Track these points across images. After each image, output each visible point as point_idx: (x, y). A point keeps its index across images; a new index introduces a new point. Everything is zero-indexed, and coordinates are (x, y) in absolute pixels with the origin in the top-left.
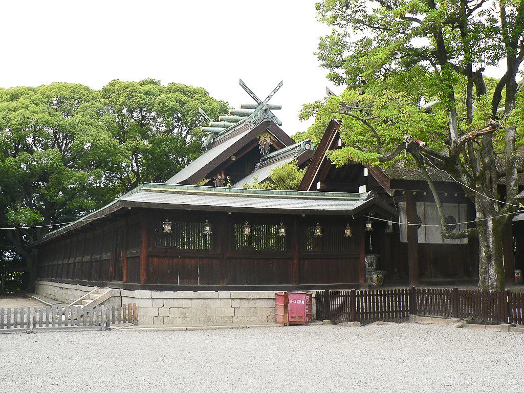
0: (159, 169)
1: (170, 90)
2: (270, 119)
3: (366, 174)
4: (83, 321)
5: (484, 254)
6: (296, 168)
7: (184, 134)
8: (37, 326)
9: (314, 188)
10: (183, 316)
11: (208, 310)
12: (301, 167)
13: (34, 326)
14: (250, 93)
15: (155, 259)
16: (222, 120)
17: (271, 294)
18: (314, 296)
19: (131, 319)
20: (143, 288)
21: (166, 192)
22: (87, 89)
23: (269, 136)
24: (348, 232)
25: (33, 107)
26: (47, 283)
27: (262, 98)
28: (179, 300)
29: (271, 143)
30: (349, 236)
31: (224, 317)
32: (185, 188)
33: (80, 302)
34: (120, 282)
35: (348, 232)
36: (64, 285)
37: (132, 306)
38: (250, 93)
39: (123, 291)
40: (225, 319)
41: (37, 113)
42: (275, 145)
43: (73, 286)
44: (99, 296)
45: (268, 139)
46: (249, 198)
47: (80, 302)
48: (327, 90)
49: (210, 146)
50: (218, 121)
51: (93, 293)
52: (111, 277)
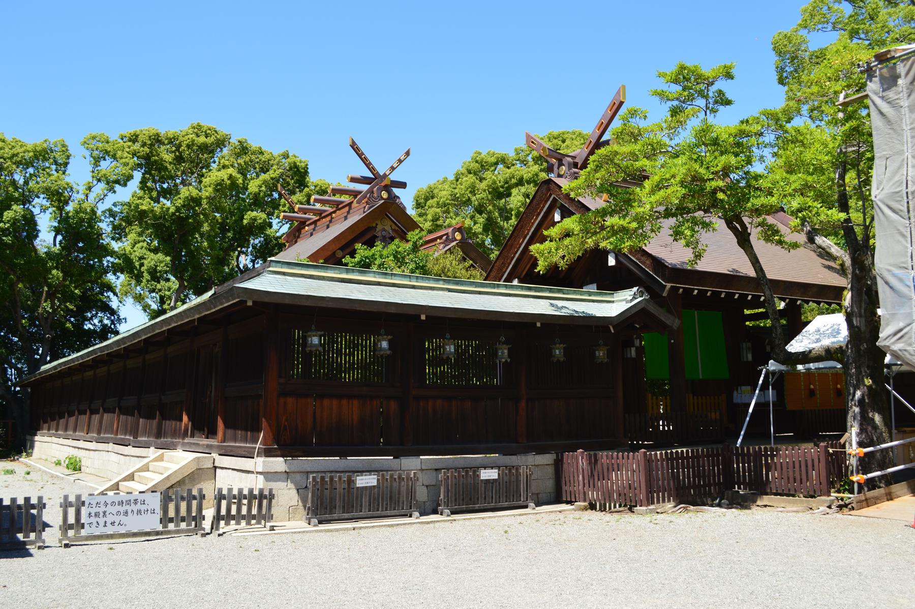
15: (290, 400)
23: (390, 223)
24: (601, 354)
33: (131, 477)
35: (601, 354)
36: (81, 444)
45: (388, 228)
48: (618, 92)
50: (294, 212)
51: (155, 460)
52: (186, 430)
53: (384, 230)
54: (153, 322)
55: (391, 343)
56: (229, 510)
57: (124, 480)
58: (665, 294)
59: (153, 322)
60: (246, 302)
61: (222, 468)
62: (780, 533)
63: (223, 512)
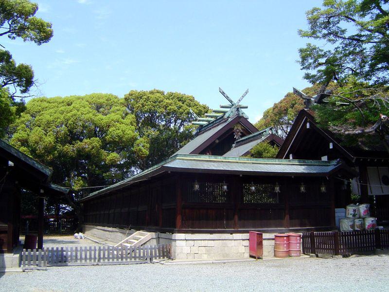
0: (220, 145)
2: (241, 115)
3: (331, 147)
4: (100, 258)
8: (102, 261)
9: (287, 157)
10: (208, 253)
11: (226, 248)
14: (227, 98)
17: (246, 236)
21: (195, 160)
22: (116, 98)
23: (240, 126)
24: (323, 189)
27: (235, 101)
28: (205, 241)
30: (324, 192)
31: (238, 253)
34: (157, 228)
35: (323, 189)
36: (106, 228)
38: (227, 98)
39: (160, 234)
40: (239, 254)
41: (50, 103)
42: (244, 133)
43: (114, 229)
45: (240, 128)
49: (197, 134)
53: (238, 129)
55: (228, 186)
56: (104, 255)
57: (124, 243)
58: (354, 161)
61: (178, 240)
63: (102, 256)
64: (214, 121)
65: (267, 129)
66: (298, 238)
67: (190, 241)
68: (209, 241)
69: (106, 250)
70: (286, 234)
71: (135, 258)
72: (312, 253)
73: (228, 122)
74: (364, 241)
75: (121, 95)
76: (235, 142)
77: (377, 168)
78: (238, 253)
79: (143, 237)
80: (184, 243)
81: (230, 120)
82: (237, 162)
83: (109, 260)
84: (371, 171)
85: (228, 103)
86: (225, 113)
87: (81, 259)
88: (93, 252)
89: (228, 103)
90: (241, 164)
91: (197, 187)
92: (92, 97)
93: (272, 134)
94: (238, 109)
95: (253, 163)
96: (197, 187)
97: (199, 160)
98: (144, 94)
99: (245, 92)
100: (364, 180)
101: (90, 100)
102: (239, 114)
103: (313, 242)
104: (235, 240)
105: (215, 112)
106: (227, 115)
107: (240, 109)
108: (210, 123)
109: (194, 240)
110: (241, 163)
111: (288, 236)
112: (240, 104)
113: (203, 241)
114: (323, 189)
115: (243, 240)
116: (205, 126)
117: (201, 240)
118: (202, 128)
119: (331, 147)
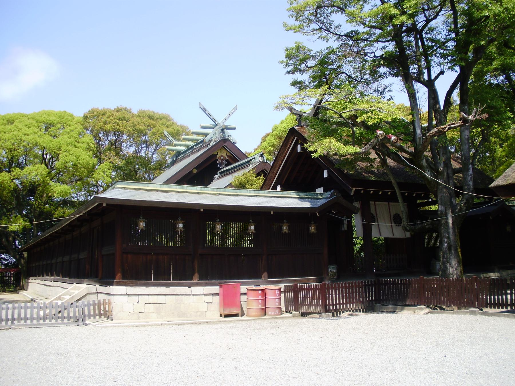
1: (139, 116)
3: (326, 175)
4: (60, 315)
5: (446, 245)
6: (254, 175)
7: (150, 154)
12: (258, 175)
13: (12, 323)
14: (209, 115)
16: (185, 140)
17: (216, 289)
18: (282, 290)
19: (105, 313)
20: (118, 284)
21: (140, 189)
22: (72, 116)
23: (226, 152)
24: (312, 229)
25: (25, 130)
26: (34, 281)
27: (220, 120)
29: (227, 158)
31: (197, 312)
32: (165, 188)
33: (59, 298)
35: (312, 229)
36: (47, 283)
37: (107, 301)
38: (209, 115)
41: (28, 135)
42: (231, 161)
44: (76, 292)
45: (225, 155)
46: (220, 196)
47: (59, 298)
49: (173, 163)
51: (71, 289)
53: (222, 156)
54: (400, 199)
56: (19, 315)
57: (55, 299)
58: (352, 194)
59: (400, 199)
60: (103, 204)
61: (117, 295)
62: (415, 334)
64: (193, 146)
65: (256, 156)
66: (278, 292)
67: (134, 297)
68: (159, 297)
69: (91, 305)
70: (262, 287)
71: (63, 318)
72: (295, 310)
73: (209, 147)
74: (388, 293)
75: (79, 112)
76: (218, 173)
77: (389, 204)
78: (197, 312)
79: (76, 292)
80: (126, 299)
81: (212, 144)
82: (198, 193)
83: (25, 322)
84: (380, 209)
85: (211, 123)
86: (206, 135)
87: (26, 319)
88: (92, 308)
89: (211, 123)
90: (204, 195)
91: (142, 224)
92: (40, 114)
93: (263, 162)
94: (223, 130)
95: (219, 194)
96: (142, 224)
97: (147, 190)
98: (109, 111)
99: (232, 108)
100: (369, 219)
101: (38, 118)
102: (224, 137)
103: (296, 298)
104: (194, 295)
105: (193, 133)
106: (209, 138)
107: (225, 131)
108: (189, 148)
109: (139, 295)
110: (203, 193)
111: (263, 291)
112: (226, 124)
113: (150, 297)
114: (313, 228)
115: (205, 295)
116: (183, 153)
117: (148, 295)
118: (179, 156)
119: (326, 175)
